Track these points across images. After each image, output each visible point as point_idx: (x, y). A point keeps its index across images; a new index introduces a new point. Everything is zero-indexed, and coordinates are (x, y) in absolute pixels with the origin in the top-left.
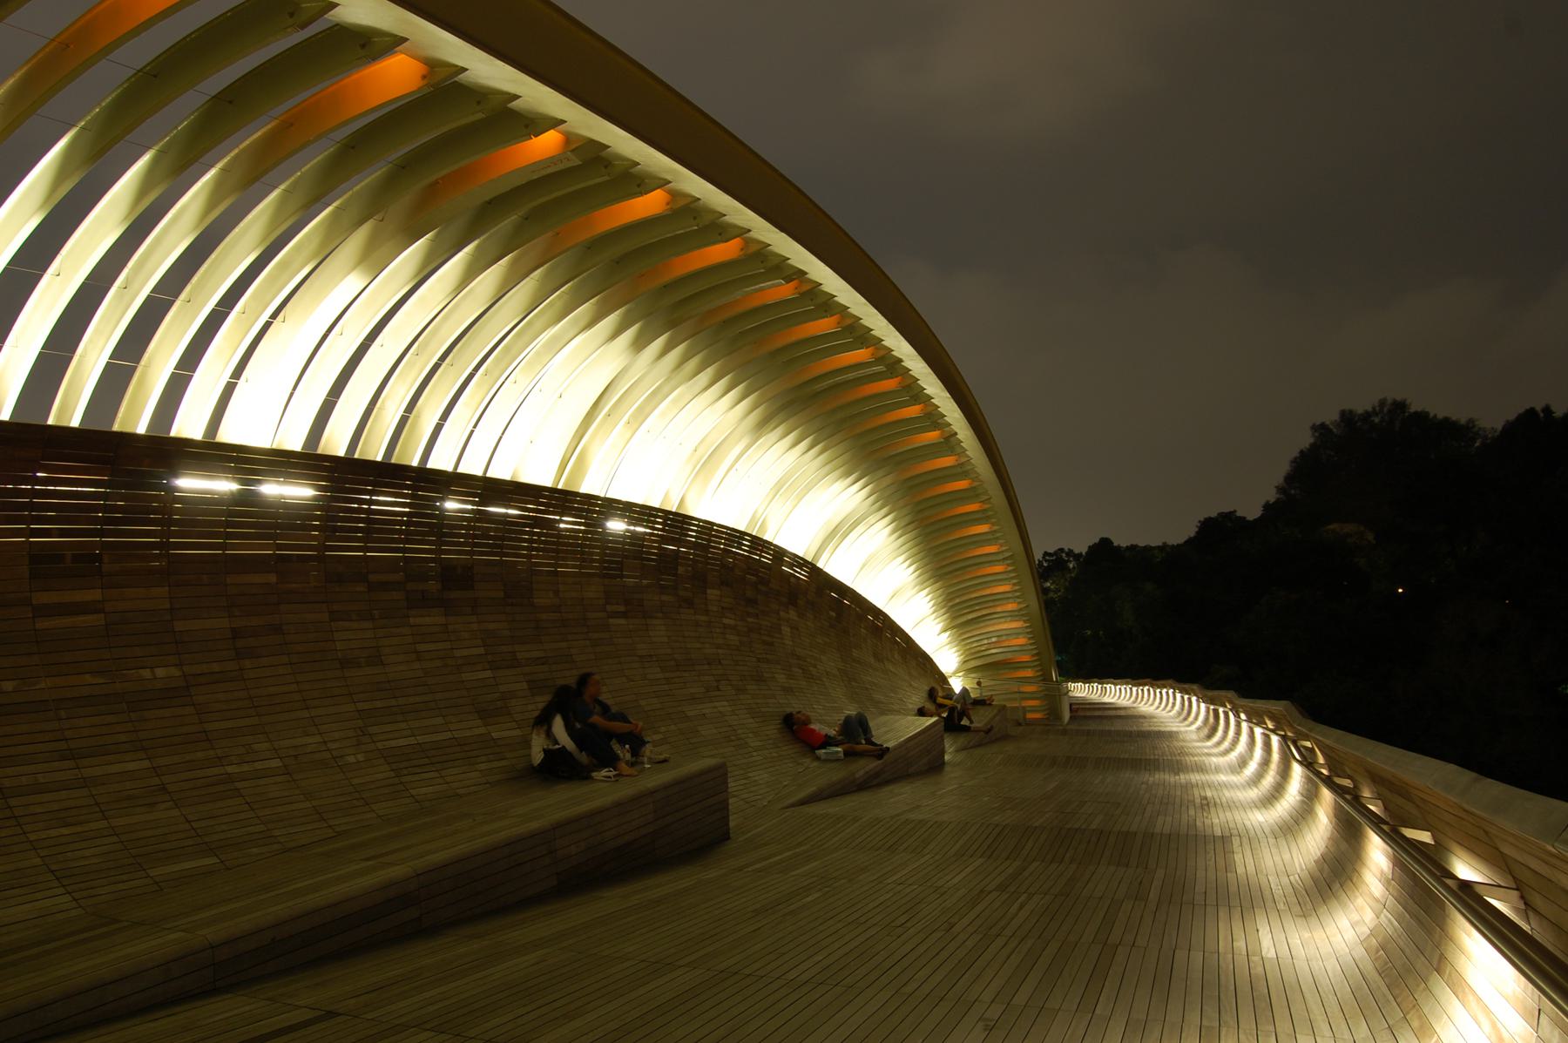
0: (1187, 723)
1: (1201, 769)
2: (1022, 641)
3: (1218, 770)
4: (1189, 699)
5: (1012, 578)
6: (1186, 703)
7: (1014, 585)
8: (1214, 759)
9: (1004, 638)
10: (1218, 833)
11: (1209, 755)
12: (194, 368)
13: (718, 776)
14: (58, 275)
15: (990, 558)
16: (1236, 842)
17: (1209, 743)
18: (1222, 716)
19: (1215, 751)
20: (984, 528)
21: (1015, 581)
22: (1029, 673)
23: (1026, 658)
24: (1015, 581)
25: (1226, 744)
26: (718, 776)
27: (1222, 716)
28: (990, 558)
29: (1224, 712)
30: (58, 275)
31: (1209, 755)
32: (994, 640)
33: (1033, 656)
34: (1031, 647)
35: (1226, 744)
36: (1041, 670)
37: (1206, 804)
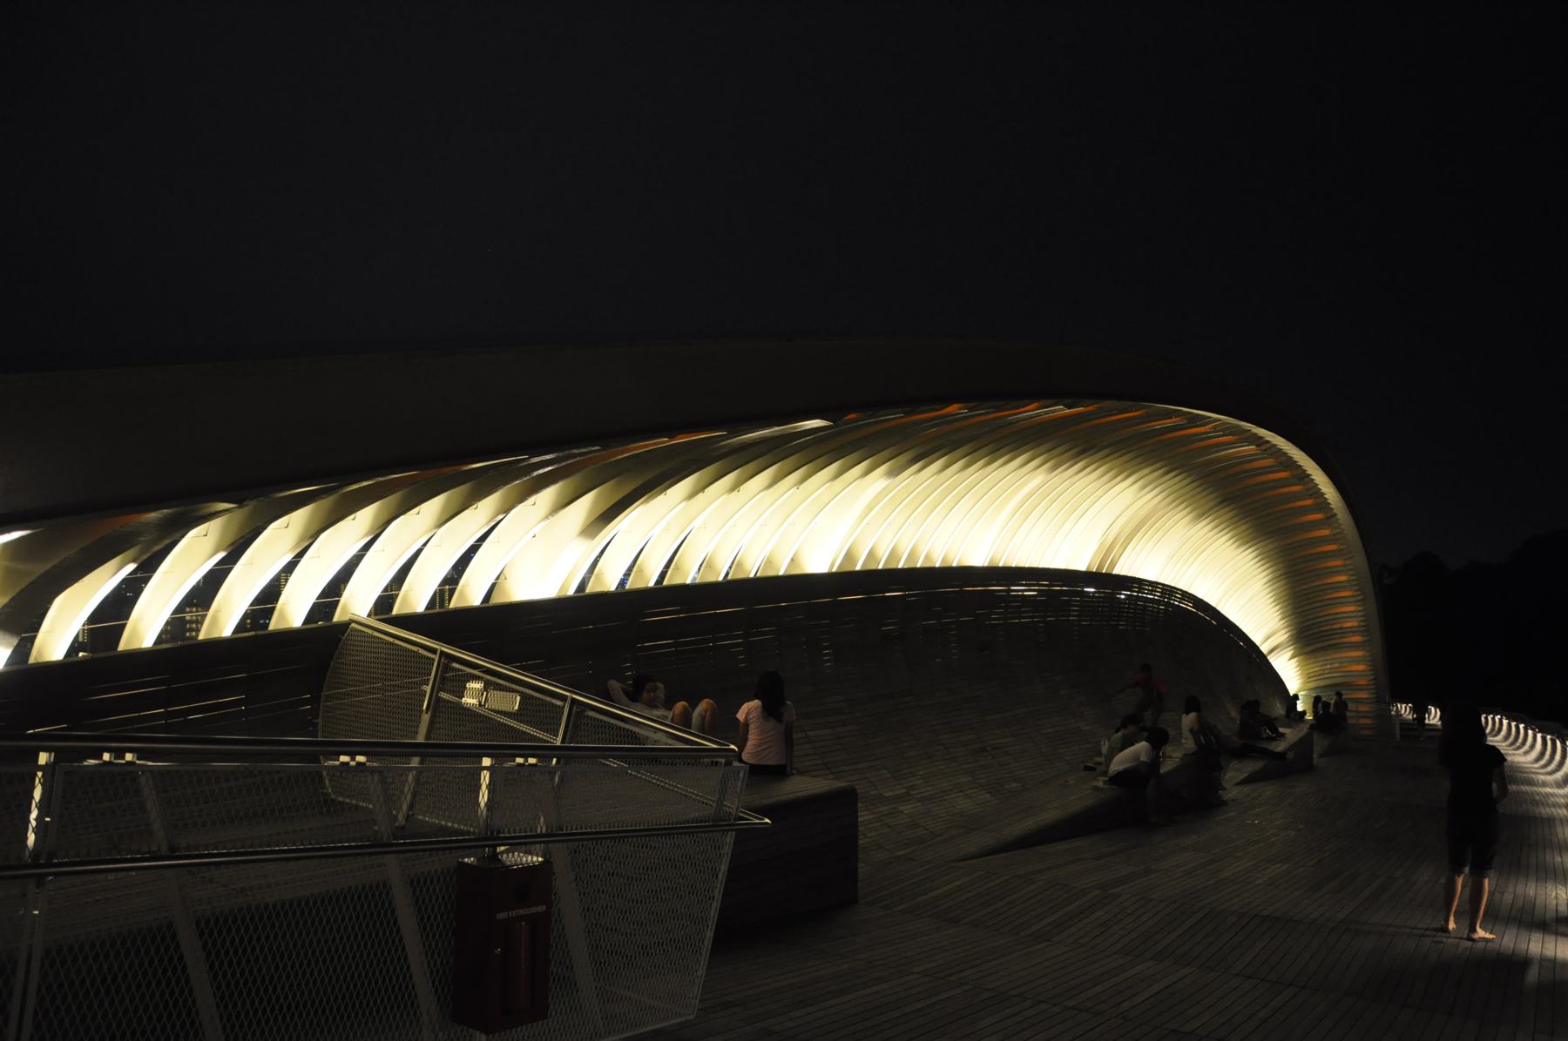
0: (1514, 747)
1: (1531, 783)
2: (1361, 667)
3: (1544, 784)
4: (1517, 728)
5: (1355, 585)
6: (1514, 729)
7: (1352, 575)
8: (1542, 777)
9: (1346, 664)
10: (1545, 816)
11: (1538, 773)
12: (368, 550)
13: (846, 799)
14: (206, 535)
15: (1345, 600)
16: (1558, 822)
17: (1536, 765)
18: (1549, 743)
19: (1549, 778)
20: (1334, 547)
21: (1352, 572)
22: (1364, 695)
23: (1363, 682)
24: (1352, 572)
25: (1553, 766)
26: (846, 799)
27: (1549, 743)
28: (1345, 600)
29: (1551, 739)
30: (206, 535)
31: (1538, 773)
32: (1336, 665)
33: (1370, 680)
34: (1369, 673)
35: (1553, 766)
36: (1373, 670)
37: (1536, 803)
